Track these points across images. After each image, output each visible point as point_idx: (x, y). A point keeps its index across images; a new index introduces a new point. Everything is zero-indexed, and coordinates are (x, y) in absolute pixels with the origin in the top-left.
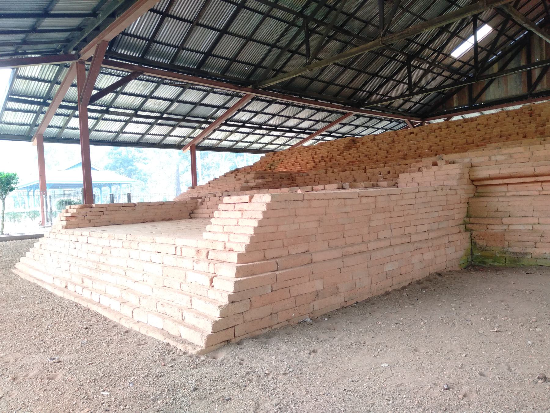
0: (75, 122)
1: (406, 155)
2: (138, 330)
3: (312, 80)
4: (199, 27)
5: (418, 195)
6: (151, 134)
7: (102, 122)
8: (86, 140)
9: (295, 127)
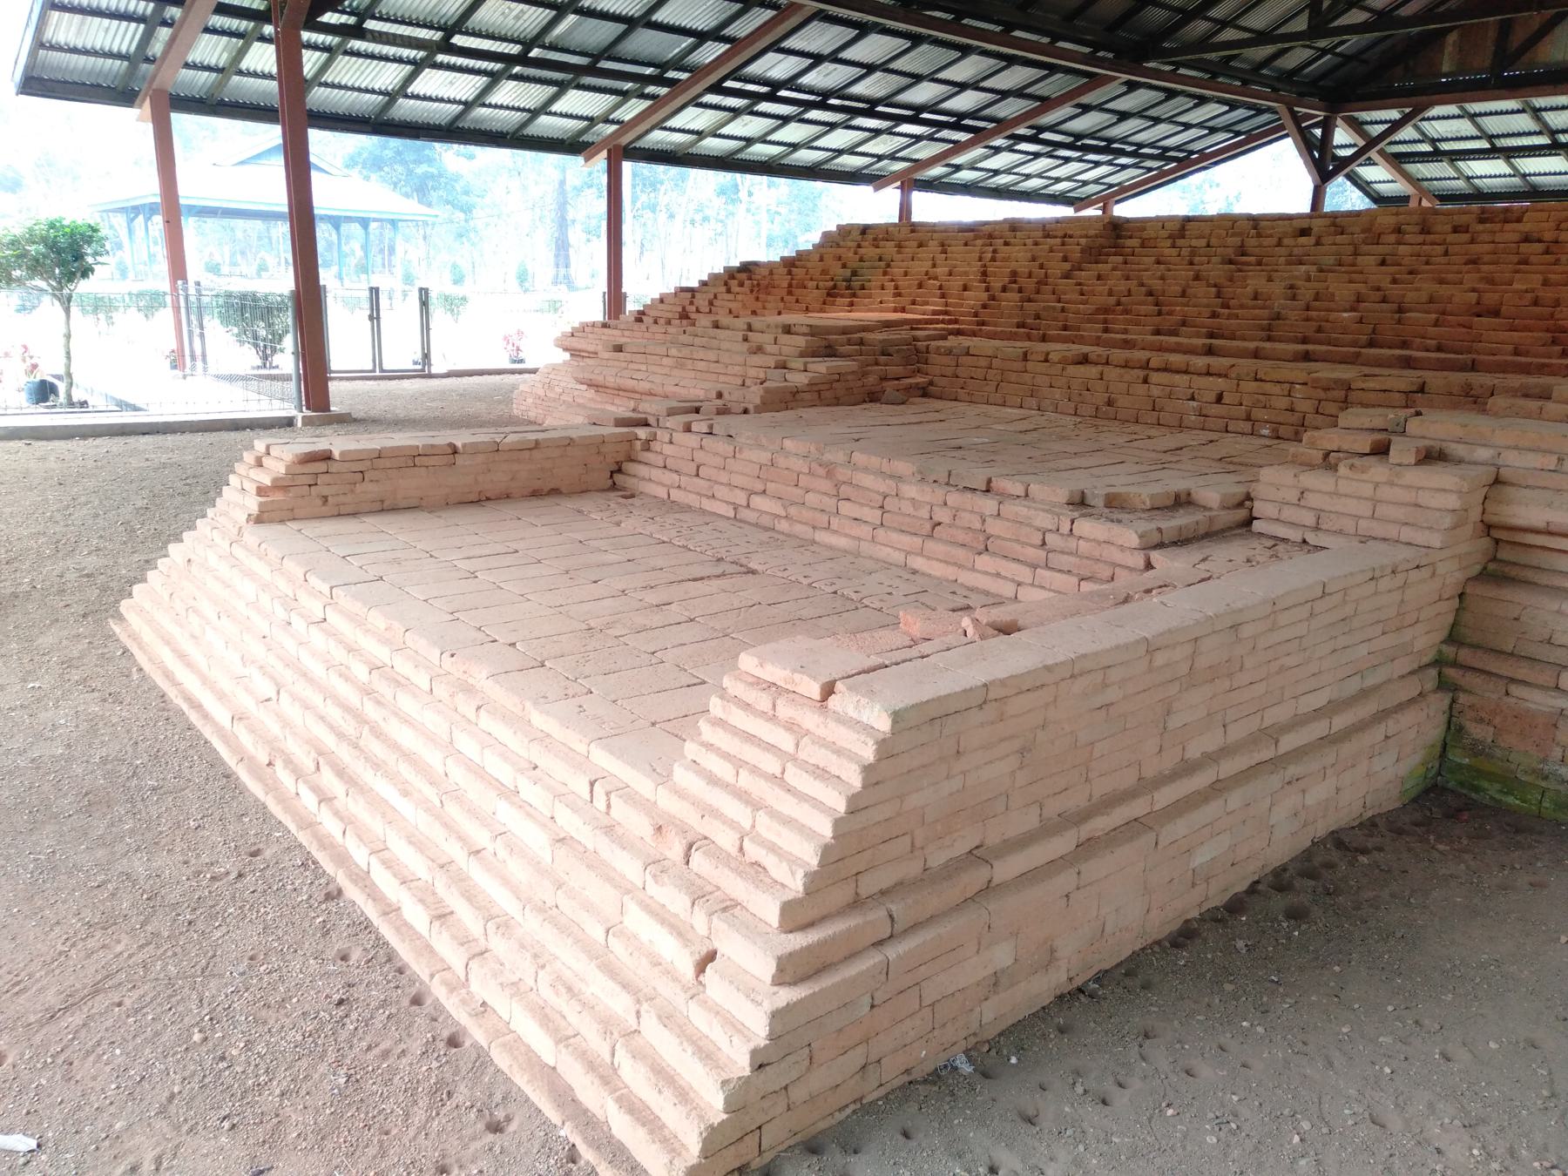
0: (263, 57)
5: (1320, 606)
6: (490, 106)
7: (342, 61)
8: (296, 113)
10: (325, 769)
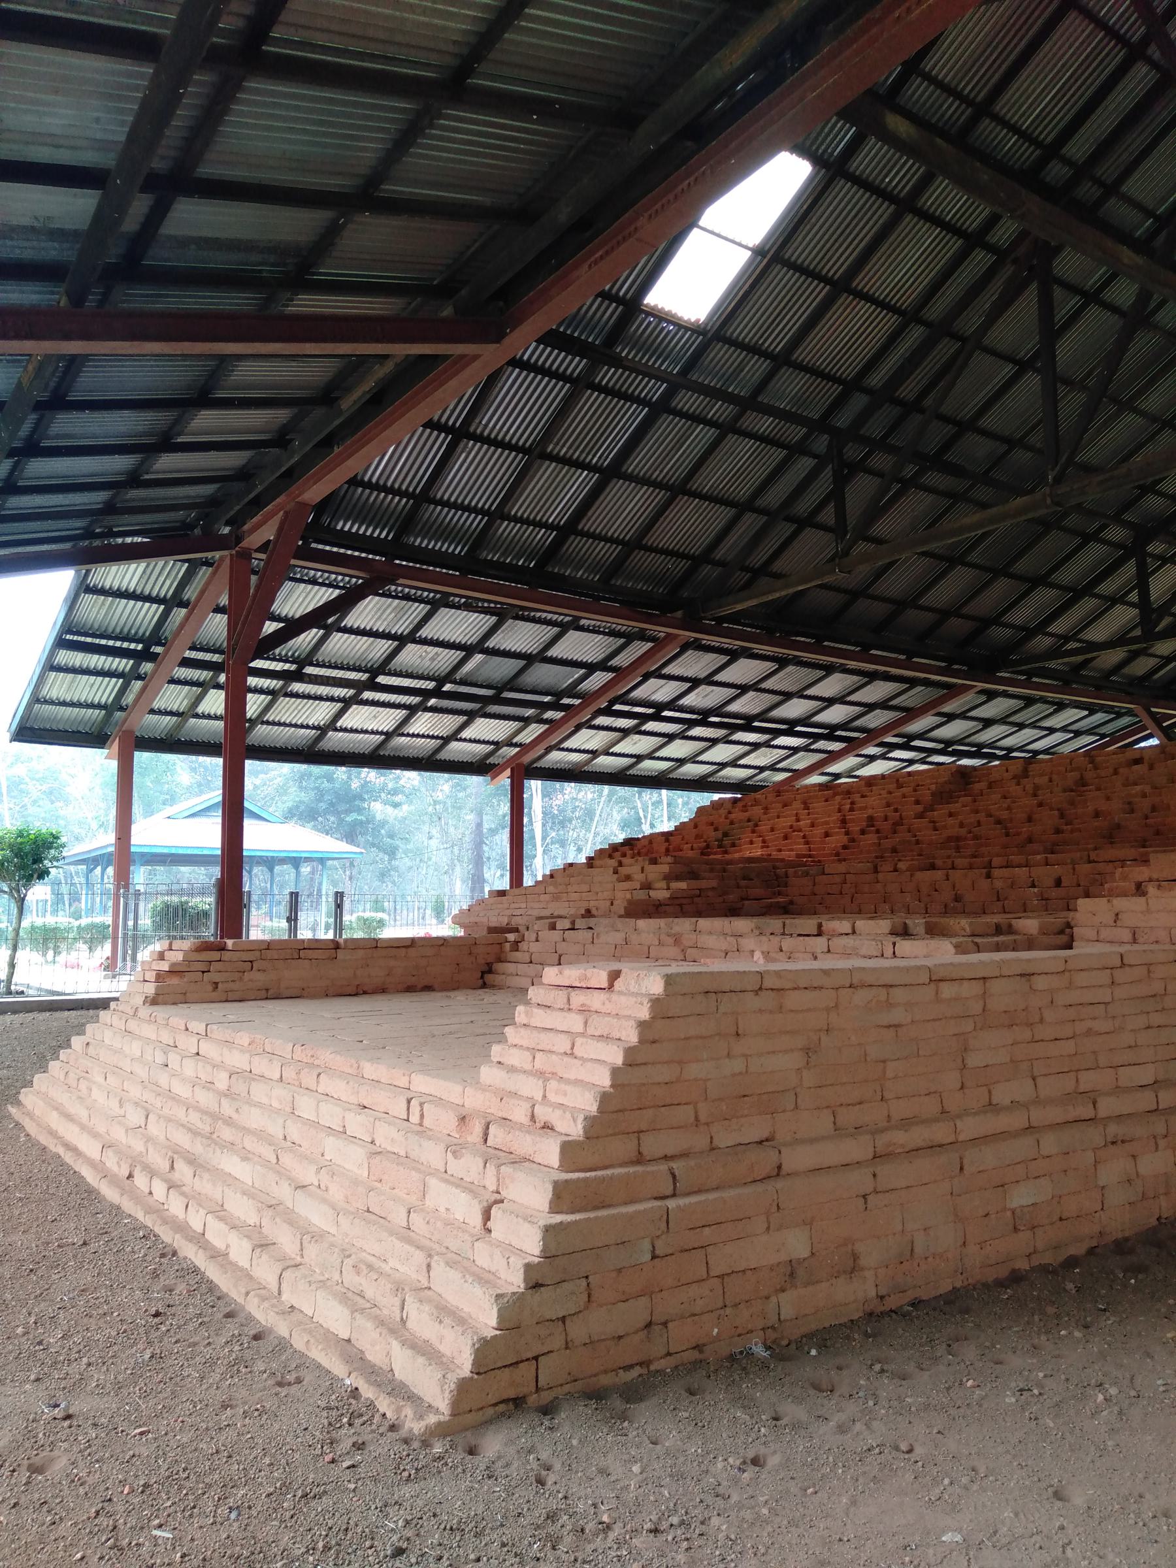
0: (215, 702)
1: (1118, 826)
2: (287, 1335)
3: (855, 595)
4: (548, 462)
5: (1120, 976)
6: (408, 735)
7: (283, 702)
8: (237, 747)
9: (805, 721)
10: (180, 1165)
